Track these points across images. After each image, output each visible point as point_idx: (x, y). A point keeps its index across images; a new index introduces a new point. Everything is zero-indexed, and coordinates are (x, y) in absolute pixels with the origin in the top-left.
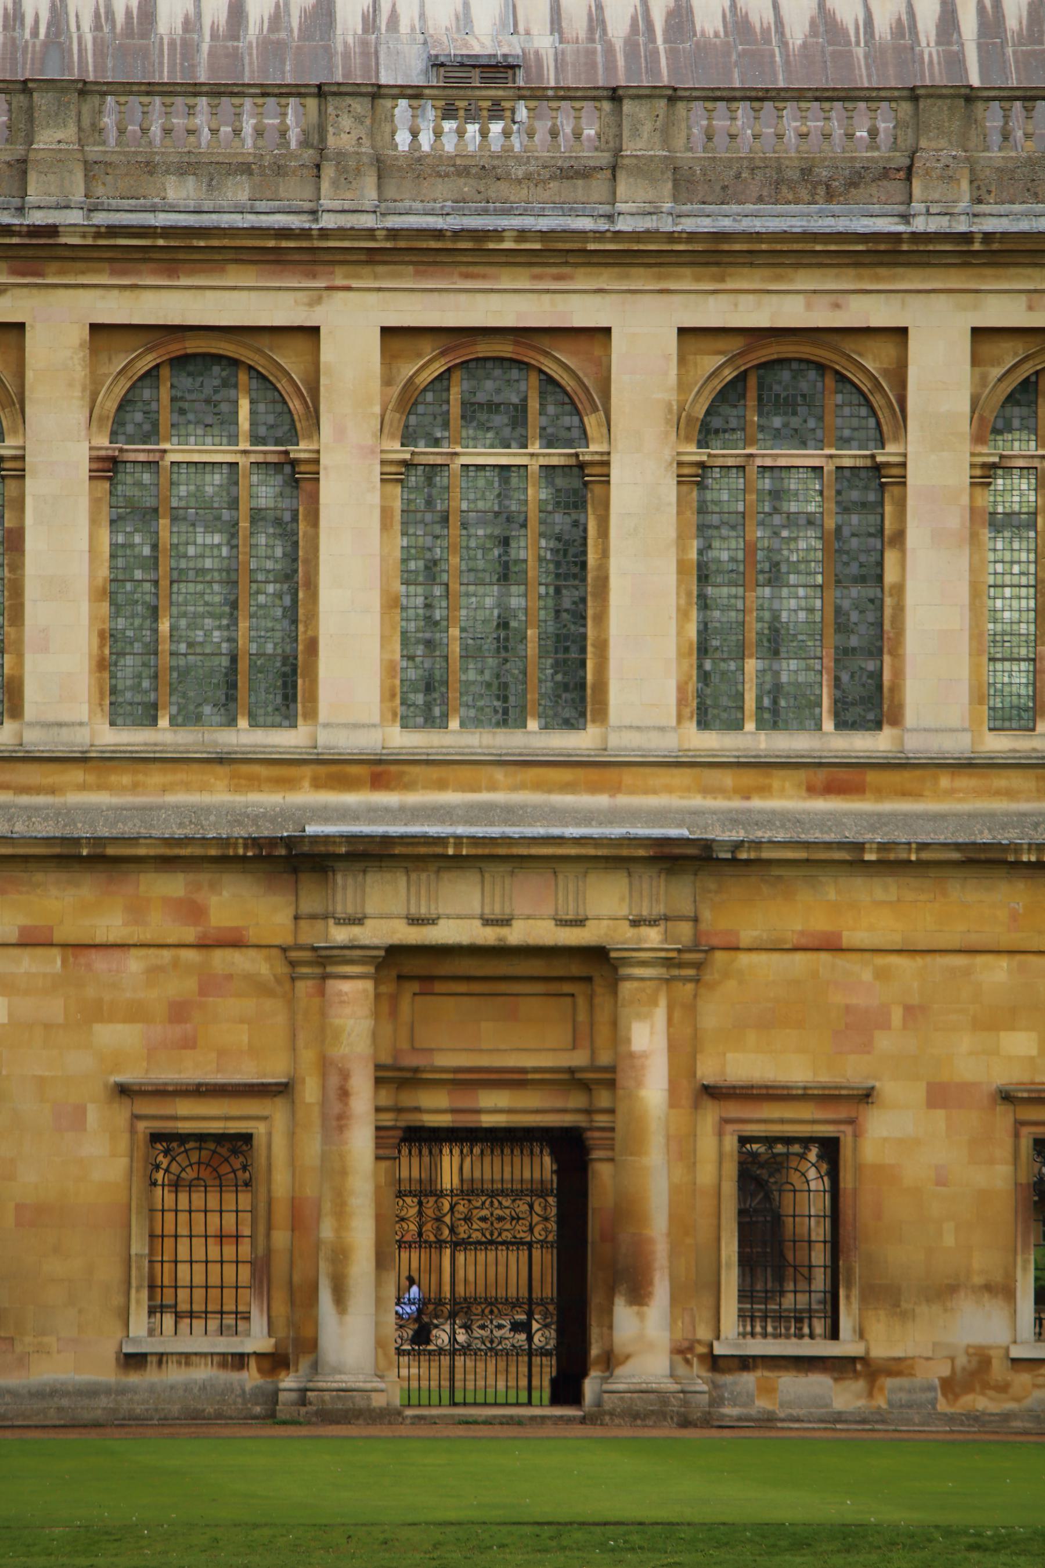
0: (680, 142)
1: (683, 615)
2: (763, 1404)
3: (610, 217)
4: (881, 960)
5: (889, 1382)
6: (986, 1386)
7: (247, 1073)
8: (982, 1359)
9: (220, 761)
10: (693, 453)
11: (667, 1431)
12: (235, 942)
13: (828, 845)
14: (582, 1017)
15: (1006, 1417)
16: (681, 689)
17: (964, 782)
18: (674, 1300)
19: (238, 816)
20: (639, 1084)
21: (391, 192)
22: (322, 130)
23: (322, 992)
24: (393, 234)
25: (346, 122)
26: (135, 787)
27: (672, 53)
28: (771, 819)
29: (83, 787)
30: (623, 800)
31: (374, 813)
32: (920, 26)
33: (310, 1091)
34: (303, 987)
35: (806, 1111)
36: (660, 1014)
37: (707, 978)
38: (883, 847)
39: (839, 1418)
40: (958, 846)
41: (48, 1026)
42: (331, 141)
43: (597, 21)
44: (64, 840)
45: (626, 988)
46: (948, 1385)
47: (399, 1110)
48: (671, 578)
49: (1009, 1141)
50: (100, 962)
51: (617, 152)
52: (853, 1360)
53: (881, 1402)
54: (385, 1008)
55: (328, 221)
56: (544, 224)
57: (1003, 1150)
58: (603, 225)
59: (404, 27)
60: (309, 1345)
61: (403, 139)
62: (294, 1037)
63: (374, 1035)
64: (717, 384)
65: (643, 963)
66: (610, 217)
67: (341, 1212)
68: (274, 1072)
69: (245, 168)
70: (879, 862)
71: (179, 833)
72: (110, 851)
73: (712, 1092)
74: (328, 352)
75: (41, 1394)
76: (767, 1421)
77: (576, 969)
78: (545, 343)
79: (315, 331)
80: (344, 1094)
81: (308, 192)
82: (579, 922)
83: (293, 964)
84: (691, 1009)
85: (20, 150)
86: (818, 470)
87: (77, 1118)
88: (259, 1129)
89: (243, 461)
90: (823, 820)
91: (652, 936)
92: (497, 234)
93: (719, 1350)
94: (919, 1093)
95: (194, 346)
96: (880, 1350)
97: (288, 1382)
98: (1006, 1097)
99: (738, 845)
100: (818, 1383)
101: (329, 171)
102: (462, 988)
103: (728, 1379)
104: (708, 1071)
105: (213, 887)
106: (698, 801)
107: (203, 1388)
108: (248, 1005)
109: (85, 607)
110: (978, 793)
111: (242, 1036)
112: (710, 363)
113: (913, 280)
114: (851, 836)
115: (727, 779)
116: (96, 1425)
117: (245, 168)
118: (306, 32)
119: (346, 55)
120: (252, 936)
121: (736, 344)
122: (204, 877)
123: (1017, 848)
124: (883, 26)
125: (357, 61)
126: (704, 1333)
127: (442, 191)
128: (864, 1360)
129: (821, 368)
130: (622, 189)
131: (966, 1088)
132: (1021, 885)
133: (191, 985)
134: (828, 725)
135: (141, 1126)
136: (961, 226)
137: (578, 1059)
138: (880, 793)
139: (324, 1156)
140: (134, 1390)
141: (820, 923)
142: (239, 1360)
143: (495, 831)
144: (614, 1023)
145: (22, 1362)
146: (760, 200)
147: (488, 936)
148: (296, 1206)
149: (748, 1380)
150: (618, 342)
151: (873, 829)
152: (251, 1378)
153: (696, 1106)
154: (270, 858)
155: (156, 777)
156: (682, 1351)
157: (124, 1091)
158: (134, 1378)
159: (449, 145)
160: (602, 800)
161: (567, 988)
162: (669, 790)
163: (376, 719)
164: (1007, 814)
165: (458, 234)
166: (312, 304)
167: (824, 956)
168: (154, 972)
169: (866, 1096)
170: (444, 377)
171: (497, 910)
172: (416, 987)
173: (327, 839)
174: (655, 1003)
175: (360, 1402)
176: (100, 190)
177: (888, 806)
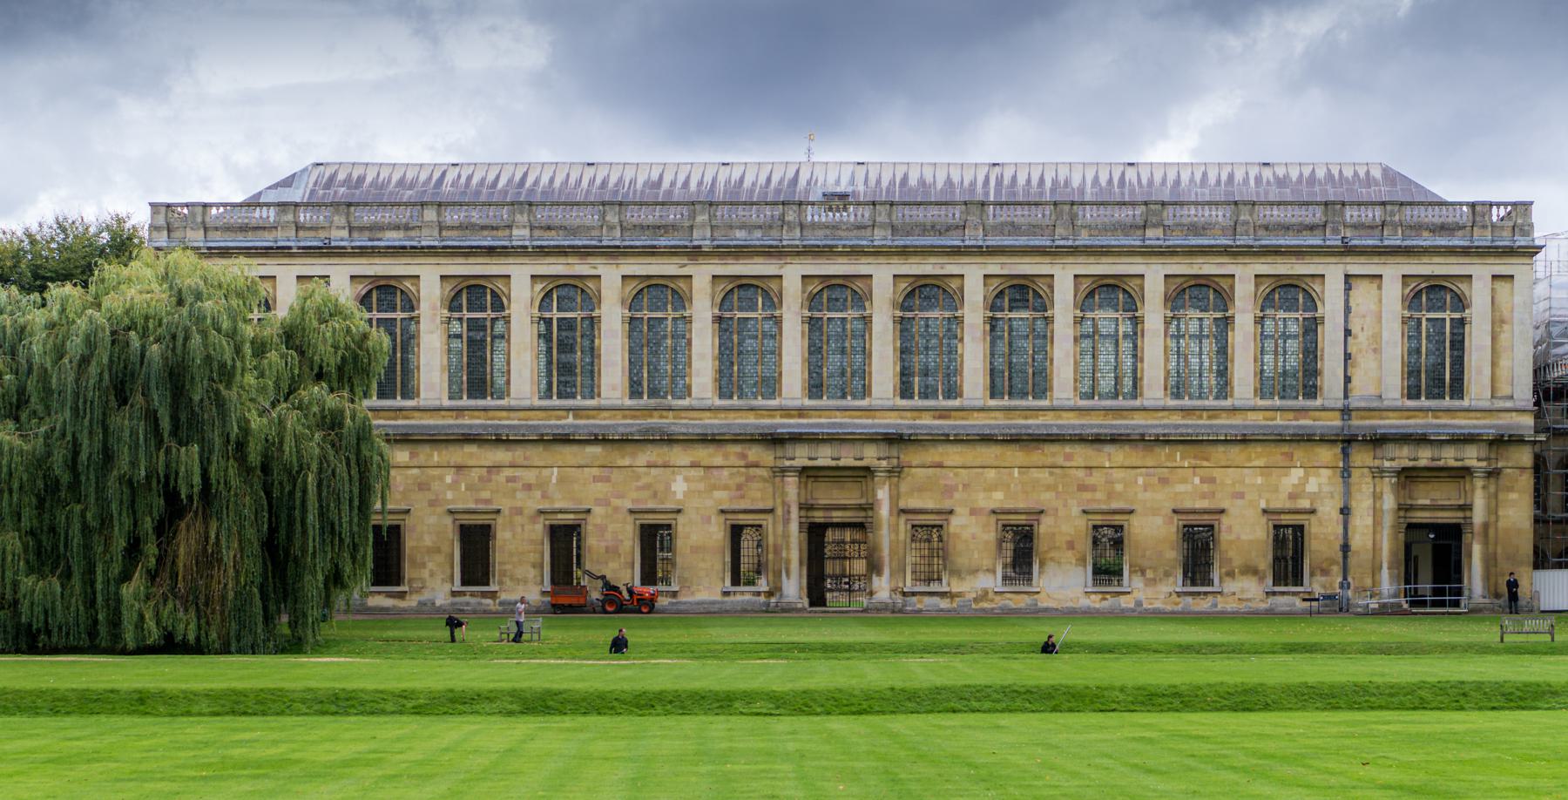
0: (894, 217)
1: (895, 363)
2: (919, 606)
3: (872, 241)
4: (956, 470)
5: (957, 599)
6: (987, 600)
7: (760, 506)
8: (986, 593)
9: (752, 410)
10: (899, 313)
11: (888, 615)
12: (757, 466)
13: (938, 435)
14: (864, 488)
15: (993, 609)
16: (895, 387)
17: (982, 414)
18: (891, 575)
19: (757, 427)
20: (880, 508)
21: (805, 233)
22: (783, 215)
23: (783, 481)
24: (804, 246)
25: (791, 213)
26: (726, 418)
27: (900, 192)
28: (922, 427)
29: (710, 418)
30: (876, 421)
31: (800, 425)
32: (800, 180)
33: (779, 512)
34: (777, 479)
35: (1023, 517)
36: (887, 487)
37: (902, 476)
38: (955, 435)
39: (942, 610)
40: (978, 435)
41: (699, 492)
42: (786, 218)
43: (879, 182)
44: (702, 434)
45: (876, 479)
46: (975, 600)
47: (807, 517)
48: (891, 352)
49: (994, 525)
50: (715, 472)
51: (875, 221)
52: (946, 593)
53: (955, 605)
54: (802, 485)
55: (785, 243)
56: (851, 243)
57: (993, 528)
58: (870, 243)
59: (819, 184)
60: (780, 589)
61: (809, 218)
62: (774, 495)
63: (799, 494)
64: (906, 292)
65: (881, 472)
66: (872, 241)
67: (788, 548)
68: (769, 505)
69: (760, 227)
70: (955, 440)
71: (739, 432)
72: (717, 438)
73: (904, 511)
74: (422, 284)
75: (698, 603)
76: (920, 611)
77: (862, 474)
78: (853, 279)
79: (781, 276)
80: (789, 512)
81: (1510, 235)
82: (861, 459)
83: (774, 472)
84: (897, 486)
85: (691, 222)
86: (1297, 319)
87: (708, 520)
88: (764, 523)
89: (760, 317)
90: (938, 427)
91: (884, 463)
92: (836, 246)
93: (905, 590)
94: (967, 511)
95: (744, 281)
96: (955, 589)
97: (773, 600)
98: (994, 512)
99: (910, 435)
100: (936, 600)
101: (785, 228)
102: (827, 479)
103: (908, 599)
104: (902, 505)
105: (750, 449)
106: (899, 421)
107: (748, 601)
108: (761, 485)
109: (710, 362)
110: (985, 418)
111: (759, 495)
112: (904, 285)
113: (511, 260)
114: (946, 432)
115: (909, 414)
116: (714, 613)
117: (760, 227)
118: (789, 186)
119: (800, 192)
120: (762, 464)
121: (1272, 280)
122: (747, 446)
123: (996, 435)
124: (966, 183)
125: (803, 194)
126: (901, 585)
127: (820, 233)
128: (950, 592)
129: (938, 287)
130: (876, 232)
131: (981, 509)
132: (999, 447)
133: (742, 479)
134: (941, 397)
135: (728, 522)
136: (980, 243)
137: (863, 501)
138: (955, 419)
139: (783, 531)
140: (727, 602)
141: (937, 459)
142: (758, 594)
143: (834, 431)
144: (873, 490)
145: (693, 593)
146: (919, 235)
147: (833, 463)
148: (775, 546)
149: (914, 599)
150: (875, 280)
151: (953, 429)
152: (762, 599)
153: (899, 515)
154: (766, 440)
155: (732, 415)
156: (894, 590)
157: (723, 511)
158: (726, 599)
159: (824, 220)
160: (870, 421)
161: (859, 479)
162: (890, 418)
163: (800, 396)
164: (721, 425)
165: (824, 246)
166: (780, 268)
167: (938, 469)
168: (732, 474)
169: (951, 512)
170: (822, 290)
171: (836, 456)
172: (813, 479)
173: (782, 434)
174: (884, 484)
175: (794, 606)
176: (715, 234)
177: (958, 422)
